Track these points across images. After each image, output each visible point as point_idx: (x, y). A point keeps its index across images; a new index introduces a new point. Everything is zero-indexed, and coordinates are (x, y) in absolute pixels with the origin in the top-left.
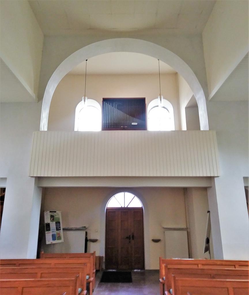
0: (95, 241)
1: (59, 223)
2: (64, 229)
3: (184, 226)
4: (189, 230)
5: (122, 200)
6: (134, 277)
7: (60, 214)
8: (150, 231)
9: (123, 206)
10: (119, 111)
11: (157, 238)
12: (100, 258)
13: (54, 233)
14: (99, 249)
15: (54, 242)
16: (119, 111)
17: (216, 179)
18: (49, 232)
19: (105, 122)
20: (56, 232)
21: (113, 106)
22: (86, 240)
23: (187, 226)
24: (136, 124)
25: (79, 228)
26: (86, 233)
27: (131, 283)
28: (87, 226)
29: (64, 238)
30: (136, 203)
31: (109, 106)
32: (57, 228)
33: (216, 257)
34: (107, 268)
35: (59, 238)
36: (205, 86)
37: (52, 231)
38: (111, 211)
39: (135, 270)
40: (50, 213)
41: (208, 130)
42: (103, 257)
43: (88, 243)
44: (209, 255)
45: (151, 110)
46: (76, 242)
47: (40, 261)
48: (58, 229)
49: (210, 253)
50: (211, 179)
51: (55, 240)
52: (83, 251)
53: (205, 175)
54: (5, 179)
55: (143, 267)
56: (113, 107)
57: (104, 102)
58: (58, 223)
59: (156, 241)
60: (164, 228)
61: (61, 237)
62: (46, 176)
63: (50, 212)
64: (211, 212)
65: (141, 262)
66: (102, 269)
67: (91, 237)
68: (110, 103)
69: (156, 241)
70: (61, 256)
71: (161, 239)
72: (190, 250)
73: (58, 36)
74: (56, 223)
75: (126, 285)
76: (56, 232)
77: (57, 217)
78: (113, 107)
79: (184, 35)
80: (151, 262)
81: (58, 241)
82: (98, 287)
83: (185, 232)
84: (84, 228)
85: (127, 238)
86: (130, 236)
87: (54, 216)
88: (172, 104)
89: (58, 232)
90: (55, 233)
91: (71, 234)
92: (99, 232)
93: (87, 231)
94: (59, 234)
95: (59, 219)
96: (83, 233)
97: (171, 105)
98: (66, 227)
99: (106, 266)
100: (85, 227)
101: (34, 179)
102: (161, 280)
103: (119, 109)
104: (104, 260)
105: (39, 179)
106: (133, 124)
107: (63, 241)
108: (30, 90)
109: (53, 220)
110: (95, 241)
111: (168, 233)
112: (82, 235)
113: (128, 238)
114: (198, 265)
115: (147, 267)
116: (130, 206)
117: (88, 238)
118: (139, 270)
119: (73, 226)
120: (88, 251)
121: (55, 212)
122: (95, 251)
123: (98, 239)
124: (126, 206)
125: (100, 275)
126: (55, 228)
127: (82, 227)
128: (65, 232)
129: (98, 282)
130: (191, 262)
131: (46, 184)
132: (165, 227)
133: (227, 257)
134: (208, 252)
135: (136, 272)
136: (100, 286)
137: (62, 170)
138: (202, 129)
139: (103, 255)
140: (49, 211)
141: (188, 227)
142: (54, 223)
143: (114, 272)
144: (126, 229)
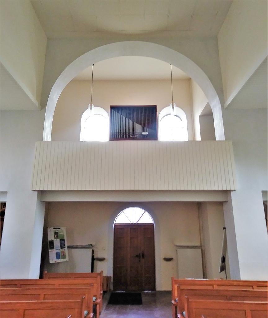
0: (102, 260)
1: (64, 240)
2: (69, 247)
3: (198, 244)
4: (203, 248)
5: (131, 216)
6: (144, 299)
7: (65, 231)
8: (162, 249)
9: (132, 223)
10: (128, 119)
11: (168, 256)
12: (108, 278)
13: (58, 251)
14: (106, 269)
15: (58, 261)
16: (128, 119)
17: (232, 193)
18: (53, 250)
19: (113, 131)
20: (60, 250)
21: (121, 114)
22: (93, 259)
23: (201, 243)
24: (146, 133)
25: (85, 246)
26: (93, 251)
27: (141, 306)
28: (93, 244)
29: (69, 256)
30: (146, 219)
31: (117, 114)
32: (61, 246)
33: (233, 278)
34: (115, 289)
35: (64, 257)
36: (221, 93)
37: (56, 249)
38: (119, 227)
39: (146, 291)
40: (54, 229)
41: (224, 140)
42: (110, 277)
43: (95, 262)
44: (225, 275)
45: (162, 119)
46: (82, 261)
47: (44, 281)
48: (62, 247)
49: (226, 272)
50: (227, 193)
51: (60, 258)
52: (90, 271)
53: (221, 189)
54: (5, 193)
55: (154, 288)
56: (121, 116)
57: (112, 110)
58: (62, 240)
59: (168, 260)
60: (176, 246)
61: (65, 255)
62: (49, 189)
63: (54, 228)
64: (227, 228)
65: (151, 282)
66: (110, 290)
67: (98, 255)
68: (119, 111)
69: (168, 260)
70: (66, 276)
71: (174, 257)
72: (205, 270)
73: (62, 39)
74: (60, 240)
75: (135, 307)
76: (60, 250)
77: (61, 233)
78: (121, 116)
79: (199, 38)
80: (162, 283)
81: (62, 259)
82: (105, 309)
83: (200, 251)
84: (90, 246)
85: (137, 256)
86: (139, 254)
87: (58, 233)
88: (185, 112)
89: (62, 250)
90: (59, 251)
91: (77, 253)
92: (106, 250)
93: (94, 249)
94: (64, 252)
95: (63, 236)
96: (89, 252)
97: (184, 113)
98: (71, 245)
99: (114, 286)
100: (91, 245)
101: (36, 193)
102: (173, 302)
103: (128, 118)
104: (112, 281)
105: (42, 193)
106: (143, 133)
107: (68, 260)
108: (32, 97)
109: (57, 237)
110: (102, 260)
111: (180, 251)
112: (88, 254)
113: (138, 256)
114: (213, 286)
115: (158, 288)
116: (139, 222)
117: (95, 257)
118: (150, 292)
119: (78, 244)
120: (94, 270)
121: (60, 228)
122: (102, 270)
123: (105, 257)
124: (135, 223)
125: (108, 296)
126: (60, 246)
127: (89, 245)
128: (69, 250)
129: (105, 304)
130: (206, 282)
131: (50, 199)
132: (178, 244)
133: (244, 277)
134: (224, 272)
135: (147, 293)
136: (107, 308)
137: (67, 183)
138: (217, 139)
139: (111, 274)
140: (53, 228)
141: (202, 244)
142: (58, 240)
143: (122, 293)
144: (135, 246)
